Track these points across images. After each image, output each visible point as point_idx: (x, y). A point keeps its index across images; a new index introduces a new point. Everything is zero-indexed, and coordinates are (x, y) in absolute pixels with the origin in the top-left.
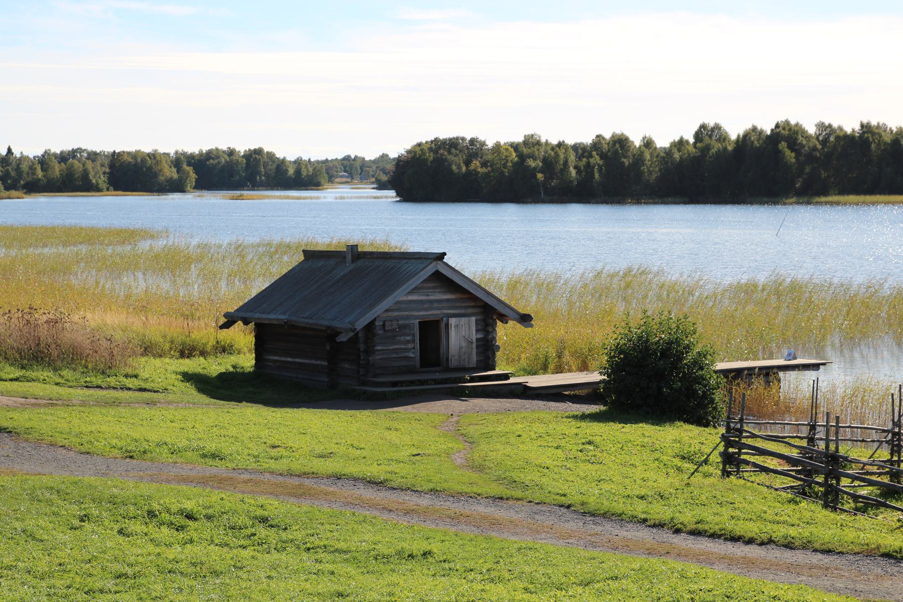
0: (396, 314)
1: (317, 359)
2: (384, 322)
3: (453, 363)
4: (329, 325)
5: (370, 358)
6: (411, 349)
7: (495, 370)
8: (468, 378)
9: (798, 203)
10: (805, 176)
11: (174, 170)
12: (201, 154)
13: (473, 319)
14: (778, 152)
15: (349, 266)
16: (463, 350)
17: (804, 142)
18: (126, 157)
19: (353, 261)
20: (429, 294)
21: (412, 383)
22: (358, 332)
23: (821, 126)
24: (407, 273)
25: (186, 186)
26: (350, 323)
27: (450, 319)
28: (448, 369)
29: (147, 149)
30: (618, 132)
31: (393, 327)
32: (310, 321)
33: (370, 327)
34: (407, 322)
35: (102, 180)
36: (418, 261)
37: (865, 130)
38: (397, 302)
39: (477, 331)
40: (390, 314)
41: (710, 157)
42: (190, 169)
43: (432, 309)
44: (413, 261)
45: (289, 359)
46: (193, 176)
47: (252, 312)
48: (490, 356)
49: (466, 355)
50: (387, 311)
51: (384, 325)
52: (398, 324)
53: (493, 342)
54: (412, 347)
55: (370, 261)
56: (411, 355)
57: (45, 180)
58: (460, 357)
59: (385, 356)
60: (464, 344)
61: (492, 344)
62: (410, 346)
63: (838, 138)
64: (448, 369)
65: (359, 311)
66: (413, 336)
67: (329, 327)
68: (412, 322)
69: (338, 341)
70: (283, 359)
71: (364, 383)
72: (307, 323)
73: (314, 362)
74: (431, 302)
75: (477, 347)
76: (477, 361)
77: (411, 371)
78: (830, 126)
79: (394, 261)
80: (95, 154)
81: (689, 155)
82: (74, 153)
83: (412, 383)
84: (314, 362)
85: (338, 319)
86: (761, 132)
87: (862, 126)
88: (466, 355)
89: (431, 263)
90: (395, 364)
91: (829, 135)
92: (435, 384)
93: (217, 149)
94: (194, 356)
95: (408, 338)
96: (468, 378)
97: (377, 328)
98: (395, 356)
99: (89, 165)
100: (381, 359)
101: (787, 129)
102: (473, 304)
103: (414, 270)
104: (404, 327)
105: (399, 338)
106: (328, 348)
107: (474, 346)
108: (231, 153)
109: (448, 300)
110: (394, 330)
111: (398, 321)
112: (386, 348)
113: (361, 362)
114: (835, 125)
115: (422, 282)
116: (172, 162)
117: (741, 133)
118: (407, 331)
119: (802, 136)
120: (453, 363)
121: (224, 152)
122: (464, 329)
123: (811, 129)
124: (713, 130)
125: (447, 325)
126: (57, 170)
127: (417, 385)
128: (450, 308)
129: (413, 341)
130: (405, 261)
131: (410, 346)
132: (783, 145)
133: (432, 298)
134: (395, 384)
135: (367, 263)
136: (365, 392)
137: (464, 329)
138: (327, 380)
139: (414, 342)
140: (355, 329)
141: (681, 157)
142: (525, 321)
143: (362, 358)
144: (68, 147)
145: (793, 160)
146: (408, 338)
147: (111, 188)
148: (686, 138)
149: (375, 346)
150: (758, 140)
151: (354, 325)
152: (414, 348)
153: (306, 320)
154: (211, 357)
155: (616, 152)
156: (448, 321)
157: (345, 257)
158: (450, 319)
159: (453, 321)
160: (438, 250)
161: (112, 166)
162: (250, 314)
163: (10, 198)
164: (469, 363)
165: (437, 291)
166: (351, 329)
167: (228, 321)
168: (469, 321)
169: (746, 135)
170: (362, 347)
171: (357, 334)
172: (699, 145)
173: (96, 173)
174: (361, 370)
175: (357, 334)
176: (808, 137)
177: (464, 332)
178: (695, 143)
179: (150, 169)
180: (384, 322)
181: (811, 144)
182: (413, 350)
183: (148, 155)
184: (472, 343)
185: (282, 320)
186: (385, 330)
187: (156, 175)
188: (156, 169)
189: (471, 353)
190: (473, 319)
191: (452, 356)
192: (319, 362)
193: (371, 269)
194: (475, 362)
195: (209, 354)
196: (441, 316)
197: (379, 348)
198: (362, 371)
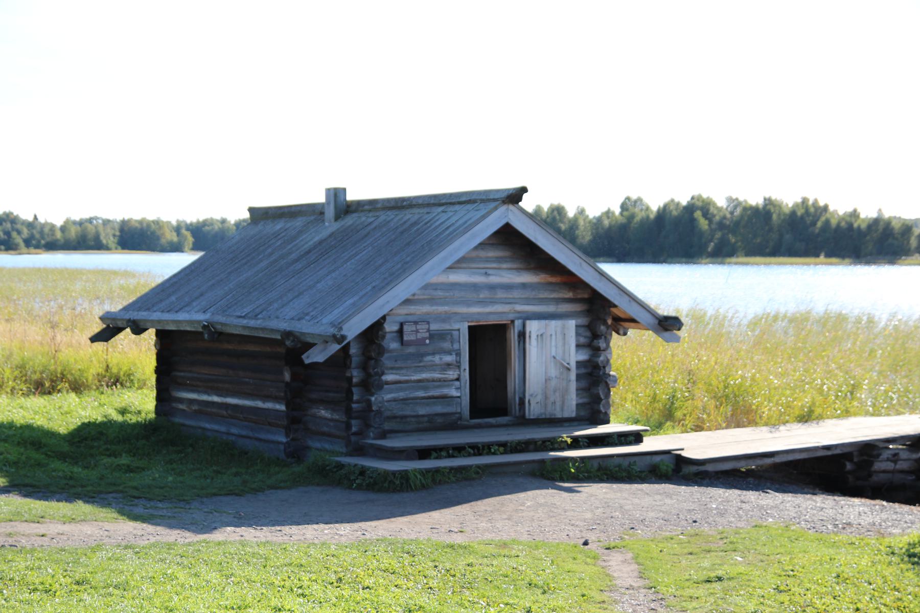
0: (425, 309)
1: (266, 398)
2: (402, 325)
3: (534, 410)
4: (288, 329)
5: (373, 399)
6: (452, 380)
7: (606, 421)
8: (569, 440)
9: (713, 263)
10: (716, 241)
11: (175, 234)
12: (198, 222)
13: (572, 324)
14: (693, 221)
15: (331, 226)
16: (553, 383)
17: (715, 212)
18: (133, 223)
19: (337, 218)
20: (490, 272)
21: (459, 450)
22: (349, 343)
23: (730, 200)
24: (448, 228)
25: (184, 248)
26: (332, 324)
27: (528, 323)
28: (524, 421)
29: (151, 217)
30: (556, 203)
31: (419, 336)
32: (252, 323)
33: (373, 333)
34: (447, 327)
35: (111, 241)
36: (469, 207)
37: (767, 202)
38: (426, 287)
39: (578, 346)
40: (412, 309)
41: (635, 224)
42: (188, 234)
43: (493, 302)
44: (457, 207)
45: (216, 399)
46: (190, 239)
47: (148, 309)
48: (602, 397)
49: (557, 394)
50: (407, 302)
51: (400, 332)
52: (429, 330)
53: (607, 369)
54: (456, 376)
55: (370, 215)
56: (454, 393)
57: (62, 241)
58: (546, 398)
59: (402, 395)
60: (553, 372)
61: (604, 373)
62: (452, 374)
63: (745, 209)
64: (524, 421)
65: (351, 301)
66: (458, 354)
67: (288, 334)
68: (456, 326)
69: (307, 361)
70: (205, 398)
71: (360, 451)
72: (244, 327)
73: (259, 404)
74: (492, 287)
75: (579, 377)
76: (577, 405)
77: (452, 424)
78: (737, 199)
79: (416, 211)
80: (109, 221)
81: (616, 222)
82: (90, 220)
83: (459, 450)
84: (259, 404)
85: (307, 318)
86: (678, 204)
87: (765, 199)
88: (557, 394)
89: (496, 208)
90: (422, 411)
91: (735, 207)
92: (505, 453)
93: (212, 219)
94: (59, 391)
95: (449, 359)
96: (569, 440)
97: (388, 336)
98: (421, 394)
99: (101, 229)
100: (395, 400)
101: (701, 200)
102: (570, 295)
103: (461, 222)
104: (440, 336)
105: (429, 358)
106: (287, 377)
107: (573, 376)
108: (224, 221)
109: (524, 286)
110: (420, 342)
111: (428, 323)
112: (406, 378)
113: (354, 406)
114: (741, 199)
115: (476, 248)
116: (173, 228)
117: (662, 205)
118: (446, 345)
119: (714, 207)
120: (534, 410)
121: (217, 221)
122: (553, 343)
123: (721, 202)
124: (636, 202)
125: (522, 335)
126: (73, 232)
127: (469, 455)
128: (528, 301)
129: (458, 366)
130: (441, 209)
131: (452, 374)
132: (698, 214)
133: (494, 279)
134: (424, 453)
135: (363, 219)
136: (363, 471)
137: (553, 343)
138: (284, 440)
139: (459, 367)
140: (343, 337)
141: (610, 224)
142: (666, 330)
143: (355, 397)
144: (86, 216)
145: (706, 227)
146: (449, 359)
147: (119, 247)
148: (612, 209)
149: (383, 374)
150: (676, 209)
151: (341, 329)
152: (458, 379)
153: (244, 322)
154: (93, 392)
155: (554, 219)
156: (524, 326)
157: (322, 213)
158: (528, 323)
159: (533, 327)
160: (507, 183)
161: (122, 230)
162: (145, 313)
163: (29, 254)
164: (562, 409)
165: (505, 266)
166: (334, 336)
167: (108, 326)
168: (563, 327)
169: (666, 207)
170: (356, 375)
171: (346, 349)
172: (625, 213)
173: (107, 235)
174: (353, 422)
175: (346, 349)
176: (720, 209)
177: (553, 349)
178: (621, 214)
179: (153, 233)
180: (402, 325)
181: (721, 214)
182: (457, 383)
183: (153, 222)
184: (569, 369)
185: (199, 322)
186: (402, 342)
187: (158, 238)
188: (159, 233)
189: (566, 391)
190: (572, 324)
191: (531, 395)
192: (269, 405)
193: (373, 226)
194: (574, 408)
195: (88, 387)
196: (511, 317)
197: (389, 377)
198: (355, 425)
